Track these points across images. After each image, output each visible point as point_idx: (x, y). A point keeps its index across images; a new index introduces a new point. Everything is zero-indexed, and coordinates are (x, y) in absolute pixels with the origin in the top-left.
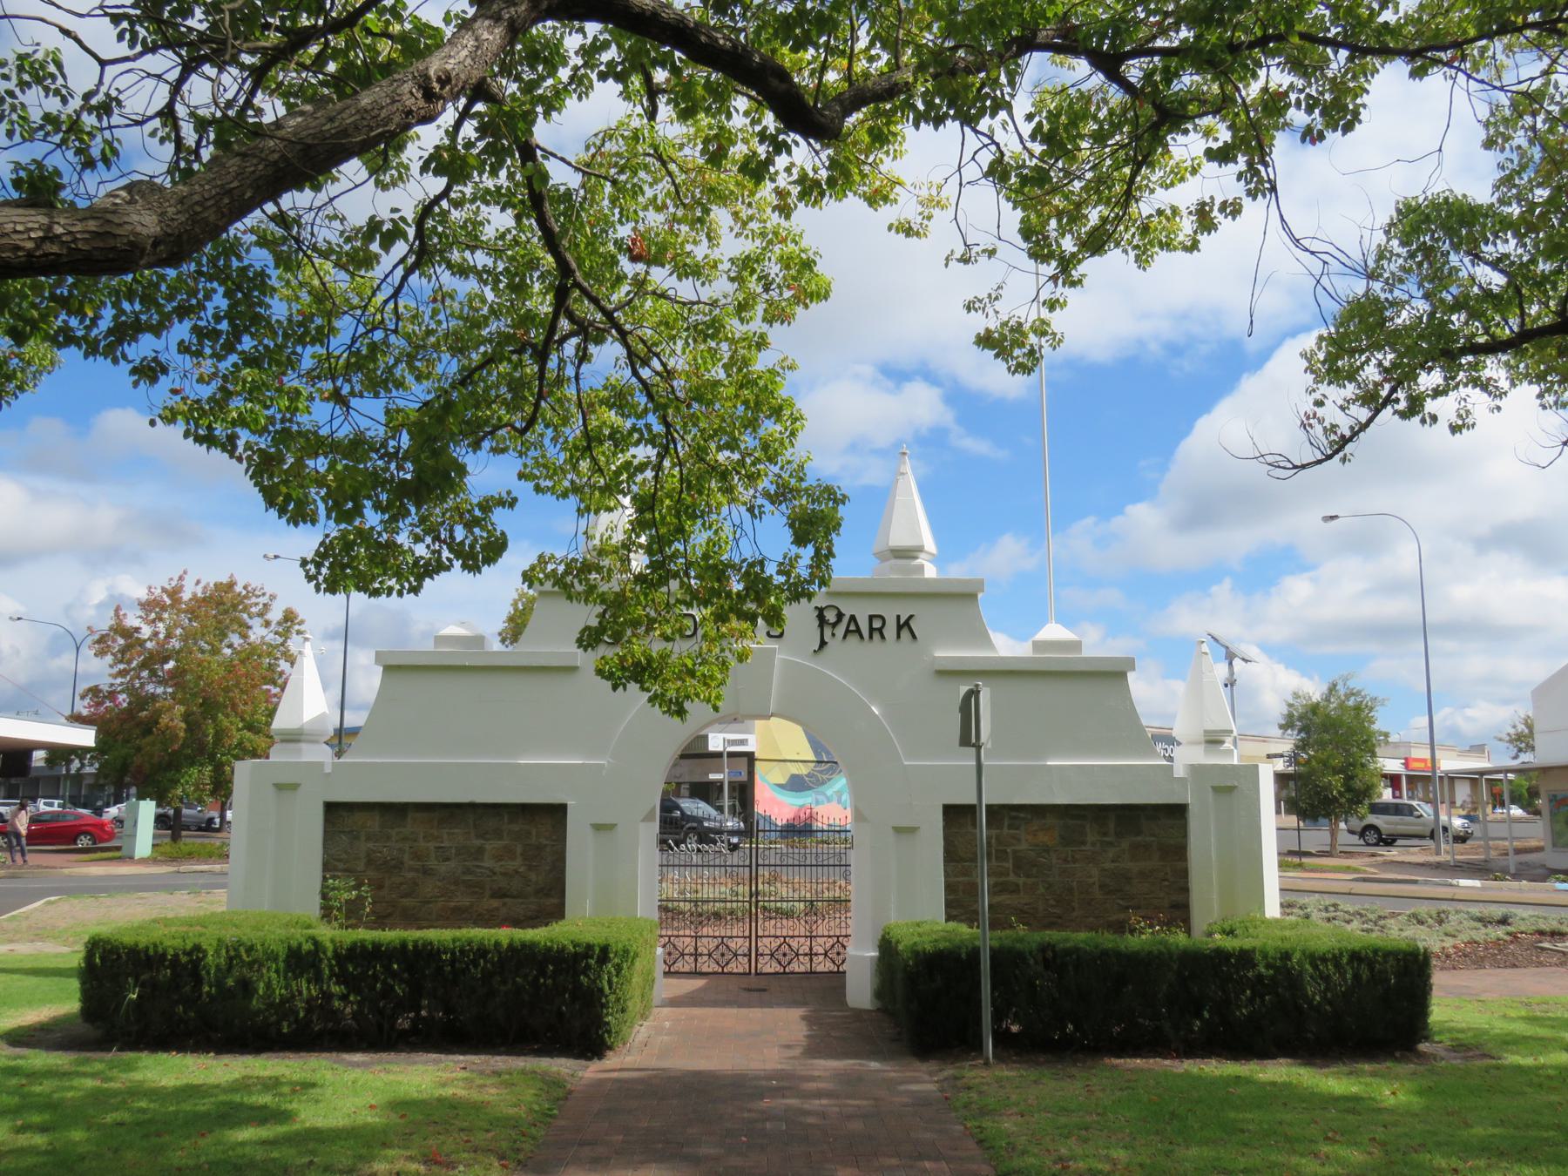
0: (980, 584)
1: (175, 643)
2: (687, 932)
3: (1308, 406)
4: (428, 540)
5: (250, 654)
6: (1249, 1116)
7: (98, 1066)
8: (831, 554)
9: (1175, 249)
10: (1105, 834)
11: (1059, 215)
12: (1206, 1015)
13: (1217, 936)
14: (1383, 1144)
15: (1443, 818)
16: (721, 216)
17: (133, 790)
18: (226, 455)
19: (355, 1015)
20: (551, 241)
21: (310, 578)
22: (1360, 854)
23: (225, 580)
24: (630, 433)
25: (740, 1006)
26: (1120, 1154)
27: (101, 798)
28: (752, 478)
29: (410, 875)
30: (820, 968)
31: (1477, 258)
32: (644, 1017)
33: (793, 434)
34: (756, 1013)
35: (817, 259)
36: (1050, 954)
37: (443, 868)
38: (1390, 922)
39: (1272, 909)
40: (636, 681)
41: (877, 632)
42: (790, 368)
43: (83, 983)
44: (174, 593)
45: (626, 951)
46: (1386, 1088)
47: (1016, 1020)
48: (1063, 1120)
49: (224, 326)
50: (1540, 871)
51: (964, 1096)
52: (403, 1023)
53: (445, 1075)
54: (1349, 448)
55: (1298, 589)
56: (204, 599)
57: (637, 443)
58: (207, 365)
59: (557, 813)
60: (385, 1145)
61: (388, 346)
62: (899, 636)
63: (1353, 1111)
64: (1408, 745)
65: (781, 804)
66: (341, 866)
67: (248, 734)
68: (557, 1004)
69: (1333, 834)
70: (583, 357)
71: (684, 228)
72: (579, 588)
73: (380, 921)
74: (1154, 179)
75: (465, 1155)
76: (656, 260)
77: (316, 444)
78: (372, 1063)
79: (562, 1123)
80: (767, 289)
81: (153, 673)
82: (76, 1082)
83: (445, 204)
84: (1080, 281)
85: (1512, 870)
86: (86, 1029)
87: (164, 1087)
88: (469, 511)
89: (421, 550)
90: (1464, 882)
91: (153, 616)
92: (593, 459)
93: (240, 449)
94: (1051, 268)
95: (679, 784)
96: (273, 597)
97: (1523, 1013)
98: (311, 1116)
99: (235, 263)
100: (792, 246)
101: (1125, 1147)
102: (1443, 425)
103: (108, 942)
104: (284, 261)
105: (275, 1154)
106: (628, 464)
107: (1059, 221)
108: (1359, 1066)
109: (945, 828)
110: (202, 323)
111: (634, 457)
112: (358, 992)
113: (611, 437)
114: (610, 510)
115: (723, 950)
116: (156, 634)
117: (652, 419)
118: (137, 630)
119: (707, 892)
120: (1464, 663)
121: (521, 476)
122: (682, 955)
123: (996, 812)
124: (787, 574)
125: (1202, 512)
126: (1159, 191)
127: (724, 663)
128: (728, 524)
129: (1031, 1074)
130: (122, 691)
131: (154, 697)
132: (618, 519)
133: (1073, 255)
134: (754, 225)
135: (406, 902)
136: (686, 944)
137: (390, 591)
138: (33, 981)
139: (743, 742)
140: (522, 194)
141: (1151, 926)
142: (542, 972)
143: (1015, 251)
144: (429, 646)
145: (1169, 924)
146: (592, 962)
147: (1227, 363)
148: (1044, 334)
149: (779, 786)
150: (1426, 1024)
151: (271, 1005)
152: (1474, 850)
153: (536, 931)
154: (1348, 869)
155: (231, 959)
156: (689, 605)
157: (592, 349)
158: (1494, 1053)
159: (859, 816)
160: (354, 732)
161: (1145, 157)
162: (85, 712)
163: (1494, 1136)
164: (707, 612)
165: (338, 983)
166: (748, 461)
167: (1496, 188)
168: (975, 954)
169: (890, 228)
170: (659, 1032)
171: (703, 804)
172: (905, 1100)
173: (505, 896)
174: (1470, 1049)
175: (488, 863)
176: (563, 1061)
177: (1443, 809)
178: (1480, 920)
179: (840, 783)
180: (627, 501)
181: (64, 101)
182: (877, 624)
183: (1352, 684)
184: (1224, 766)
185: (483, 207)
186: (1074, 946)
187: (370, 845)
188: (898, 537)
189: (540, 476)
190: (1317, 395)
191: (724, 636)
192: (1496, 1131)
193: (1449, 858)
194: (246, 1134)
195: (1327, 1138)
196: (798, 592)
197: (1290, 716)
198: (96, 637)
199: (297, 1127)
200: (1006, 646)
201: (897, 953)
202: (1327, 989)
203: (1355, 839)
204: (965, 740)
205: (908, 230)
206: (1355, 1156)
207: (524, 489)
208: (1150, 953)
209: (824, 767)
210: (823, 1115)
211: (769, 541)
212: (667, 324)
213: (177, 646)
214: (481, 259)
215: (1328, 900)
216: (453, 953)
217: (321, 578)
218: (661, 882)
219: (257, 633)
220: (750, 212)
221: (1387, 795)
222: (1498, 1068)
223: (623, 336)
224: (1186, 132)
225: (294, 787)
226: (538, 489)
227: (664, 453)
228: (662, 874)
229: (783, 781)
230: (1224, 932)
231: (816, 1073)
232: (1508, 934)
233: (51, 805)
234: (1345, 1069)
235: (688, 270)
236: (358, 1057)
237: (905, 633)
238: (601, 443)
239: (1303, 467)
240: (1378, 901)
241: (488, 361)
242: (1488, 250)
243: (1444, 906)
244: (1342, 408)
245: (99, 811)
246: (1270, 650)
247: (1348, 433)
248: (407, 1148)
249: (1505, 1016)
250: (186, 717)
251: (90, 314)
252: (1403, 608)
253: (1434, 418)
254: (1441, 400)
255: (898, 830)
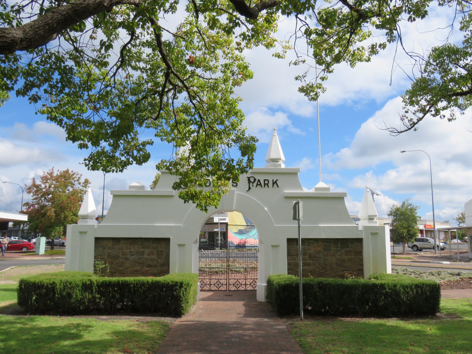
0: (298, 170)
1: (52, 190)
2: (207, 278)
3: (403, 113)
4: (125, 155)
5: (75, 193)
6: (386, 337)
7: (23, 320)
8: (253, 159)
9: (363, 61)
10: (337, 248)
11: (326, 50)
12: (370, 304)
13: (373, 279)
14: (429, 346)
15: (437, 243)
16: (219, 52)
17: (40, 234)
18: (59, 126)
19: (103, 304)
20: (164, 59)
21: (86, 165)
22: (412, 254)
23: (65, 170)
24: (190, 121)
25: (224, 300)
26: (345, 349)
27: (30, 236)
28: (229, 135)
29: (122, 260)
30: (248, 289)
31: (457, 65)
32: (194, 304)
33: (241, 121)
34: (229, 303)
35: (249, 66)
36: (321, 285)
37: (132, 258)
38: (423, 275)
39: (389, 271)
40: (192, 200)
41: (266, 185)
42: (240, 100)
43: (18, 294)
44: (51, 174)
45: (188, 284)
46: (428, 328)
47: (310, 306)
48: (326, 338)
49: (59, 85)
50: (467, 259)
51: (295, 330)
52: (119, 306)
53: (131, 323)
54: (416, 126)
55: (392, 174)
56: (60, 176)
57: (192, 124)
58: (54, 98)
59: (167, 241)
60: (111, 346)
61: (112, 92)
62: (273, 186)
63: (418, 335)
64: (425, 221)
65: (235, 238)
66: (100, 257)
67: (74, 217)
68: (167, 300)
69: (404, 248)
70: (175, 97)
71: (208, 56)
72: (174, 170)
73: (112, 274)
74: (356, 38)
75: (137, 350)
76: (198, 67)
77: (87, 123)
78: (108, 319)
79: (168, 338)
80: (233, 75)
81: (45, 198)
82: (15, 325)
83: (129, 45)
84: (332, 71)
85: (459, 259)
86: (19, 308)
87: (43, 327)
88: (138, 146)
89: (123, 158)
90: (444, 262)
91: (45, 181)
92: (178, 130)
93: (63, 124)
94: (323, 67)
95: (205, 232)
96: (81, 175)
97: (468, 304)
98: (88, 337)
99: (63, 65)
100: (241, 62)
101: (347, 347)
102: (446, 119)
103: (26, 281)
104: (78, 64)
105: (76, 349)
106: (189, 131)
107: (326, 52)
108: (418, 320)
109: (288, 245)
110: (52, 83)
111: (191, 129)
112: (104, 296)
113: (184, 122)
114: (184, 146)
115: (218, 283)
116: (46, 187)
117: (197, 117)
118: (40, 185)
119: (213, 265)
120: (442, 196)
121: (156, 135)
122: (206, 284)
123: (304, 240)
124: (239, 165)
125: (363, 151)
126: (358, 43)
127: (219, 194)
128: (221, 149)
129: (316, 323)
130: (36, 204)
131: (46, 206)
132: (185, 150)
133: (331, 62)
134: (230, 55)
135: (120, 268)
136: (207, 281)
137: (113, 171)
138: (5, 292)
139: (224, 219)
140: (155, 42)
141: (352, 276)
142: (162, 291)
143: (312, 61)
144: (127, 189)
145: (357, 275)
146: (178, 287)
147: (371, 107)
148: (320, 88)
149: (236, 233)
150: (439, 307)
151: (77, 301)
152: (447, 252)
153: (160, 278)
154: (409, 258)
155: (64, 286)
156: (208, 176)
157: (178, 95)
158: (460, 316)
159: (261, 242)
160: (105, 216)
161: (354, 30)
162: (25, 211)
163: (464, 344)
164: (214, 178)
165: (98, 294)
166: (227, 130)
167: (463, 43)
168: (297, 285)
169: (273, 56)
170: (199, 309)
171: (213, 239)
172: (276, 331)
173: (151, 266)
174: (452, 315)
175: (146, 256)
176: (168, 318)
177: (437, 240)
178: (451, 274)
179: (254, 232)
180: (188, 142)
181: (5, 8)
182: (266, 182)
183: (409, 202)
184: (374, 227)
185: (142, 48)
186: (326, 282)
187: (109, 251)
188: (273, 155)
189: (161, 135)
190: (406, 110)
191: (220, 186)
192: (465, 342)
193: (439, 255)
194: (67, 343)
195: (411, 345)
196: (243, 171)
197: (391, 212)
198: (28, 188)
199: (83, 340)
200: (306, 190)
201: (273, 284)
202: (408, 296)
203: (410, 249)
204: (295, 218)
205: (279, 56)
206: (421, 350)
207: (157, 140)
208: (352, 285)
209: (249, 227)
210: (250, 336)
211: (234, 154)
212: (201, 87)
213: (52, 190)
214: (142, 65)
215: (404, 268)
216: (134, 285)
217: (90, 165)
218: (199, 262)
219: (78, 187)
220: (229, 51)
221: (419, 236)
222: (462, 321)
223: (187, 88)
224: (367, 22)
225: (85, 233)
226: (162, 139)
227: (200, 127)
228: (199, 259)
229: (236, 231)
230: (374, 278)
231: (248, 322)
232: (460, 278)
233: (15, 238)
234: (414, 321)
235: (208, 69)
236: (104, 317)
237: (275, 185)
238: (180, 124)
239: (401, 132)
240: (419, 268)
241: (145, 98)
242: (461, 63)
243: (440, 270)
244: (414, 114)
245: (30, 240)
246: (385, 193)
247: (416, 121)
248: (118, 347)
249: (462, 304)
250: (55, 212)
251: (14, 79)
252: (425, 180)
253: (444, 116)
254: (445, 111)
255: (273, 246)
